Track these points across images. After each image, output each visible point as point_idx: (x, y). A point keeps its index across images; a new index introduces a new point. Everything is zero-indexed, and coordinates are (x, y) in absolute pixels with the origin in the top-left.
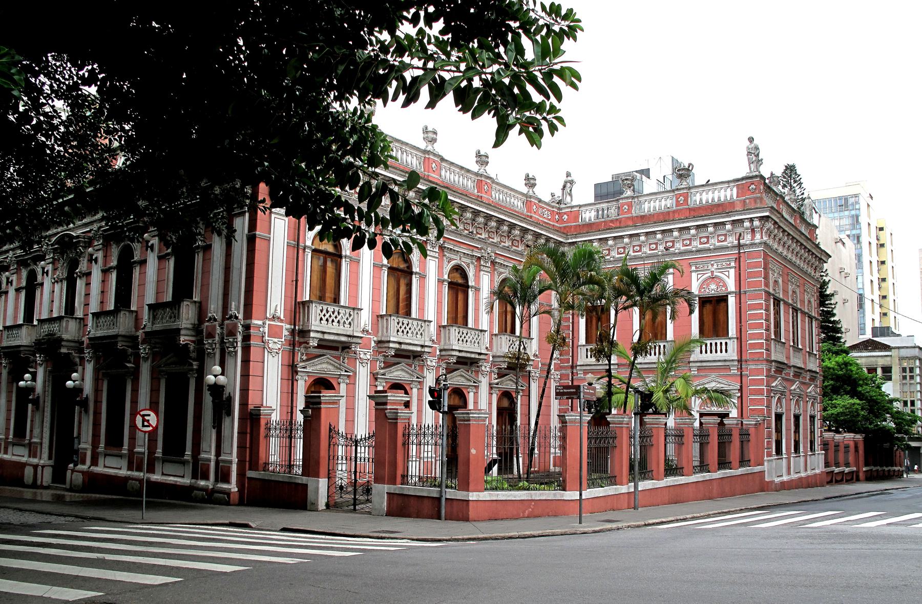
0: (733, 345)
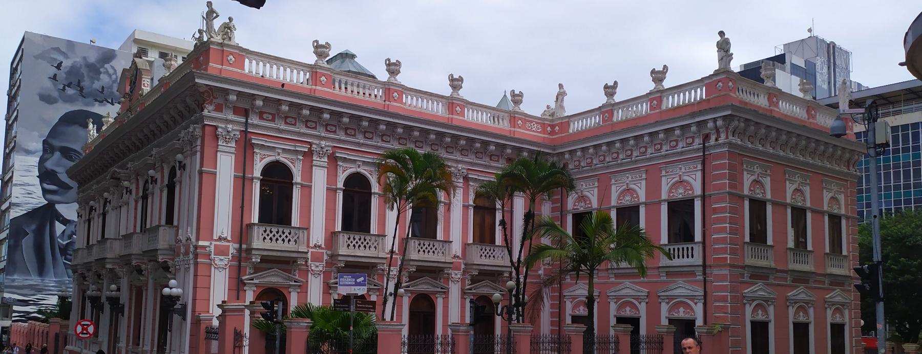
0: (698, 250)
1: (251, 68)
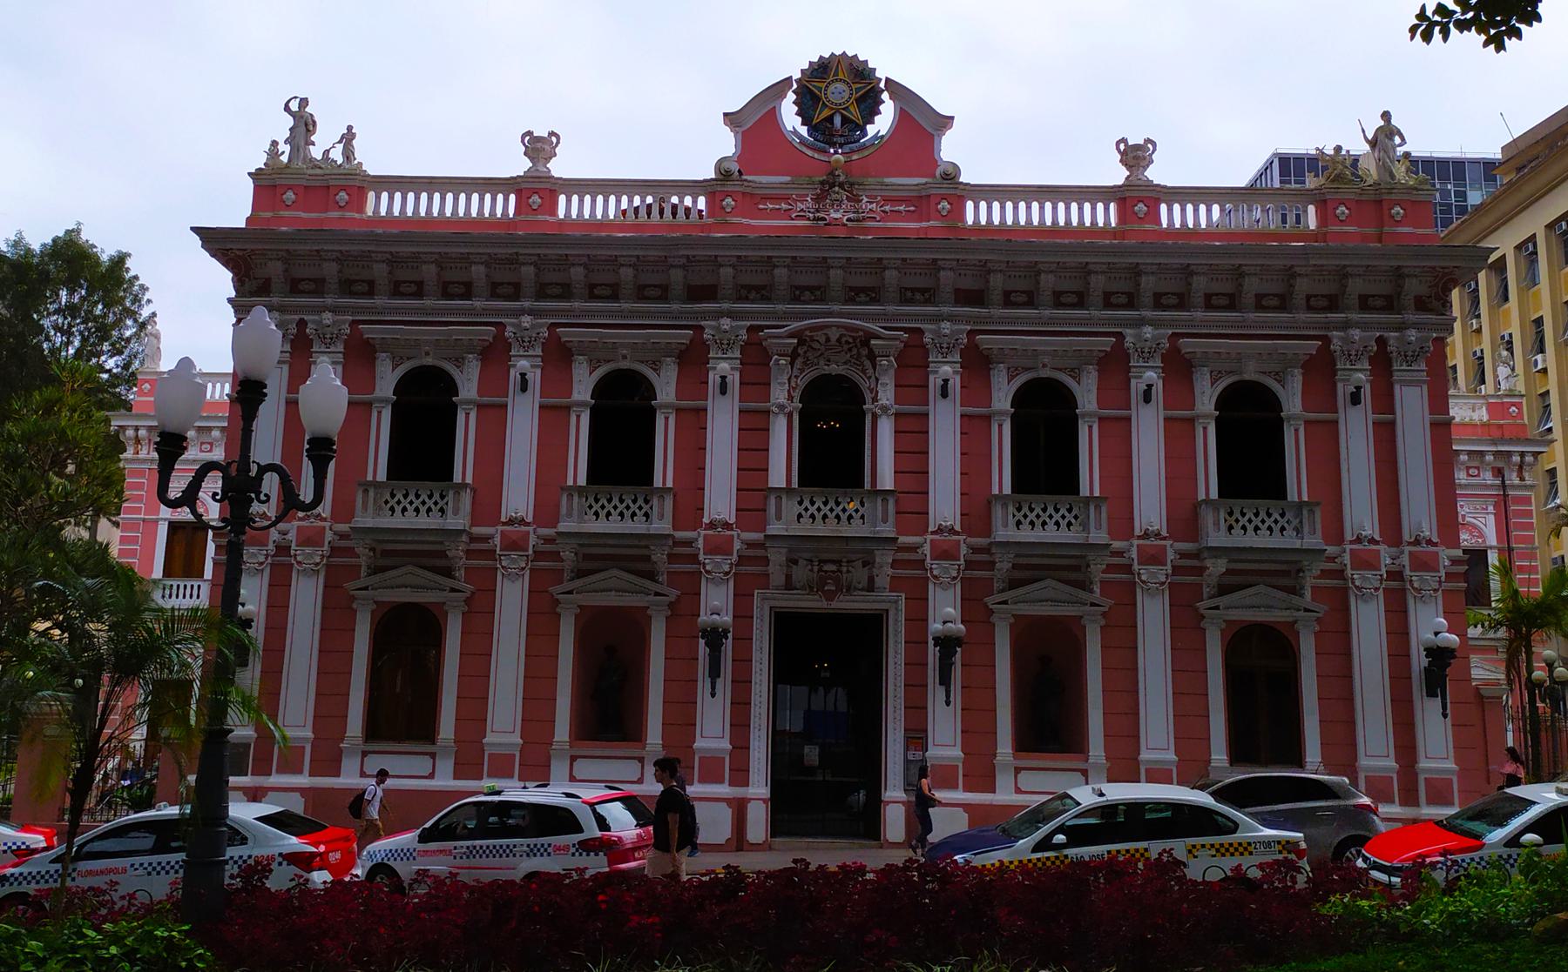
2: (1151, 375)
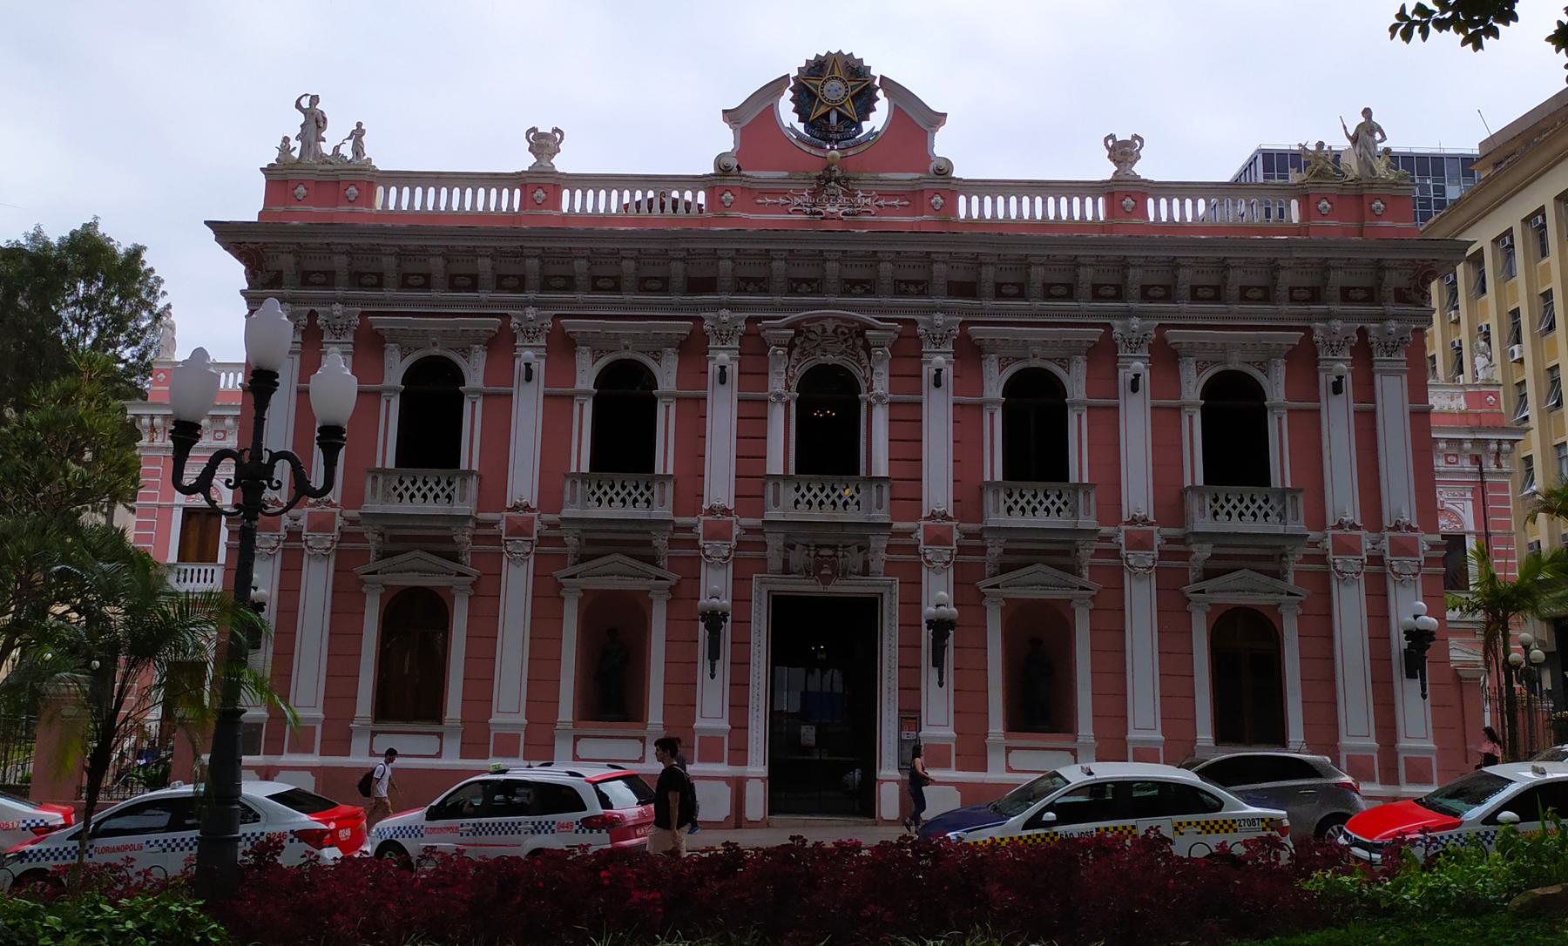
1: (391, 199)
2: (1138, 365)
